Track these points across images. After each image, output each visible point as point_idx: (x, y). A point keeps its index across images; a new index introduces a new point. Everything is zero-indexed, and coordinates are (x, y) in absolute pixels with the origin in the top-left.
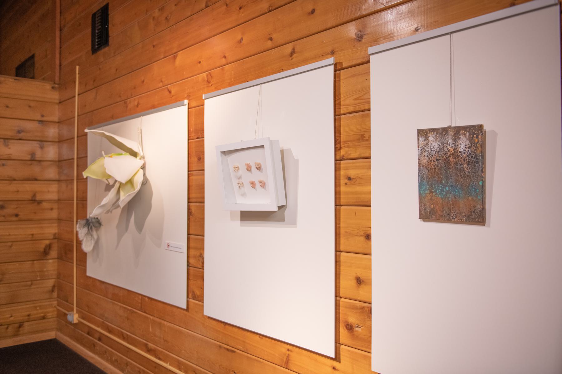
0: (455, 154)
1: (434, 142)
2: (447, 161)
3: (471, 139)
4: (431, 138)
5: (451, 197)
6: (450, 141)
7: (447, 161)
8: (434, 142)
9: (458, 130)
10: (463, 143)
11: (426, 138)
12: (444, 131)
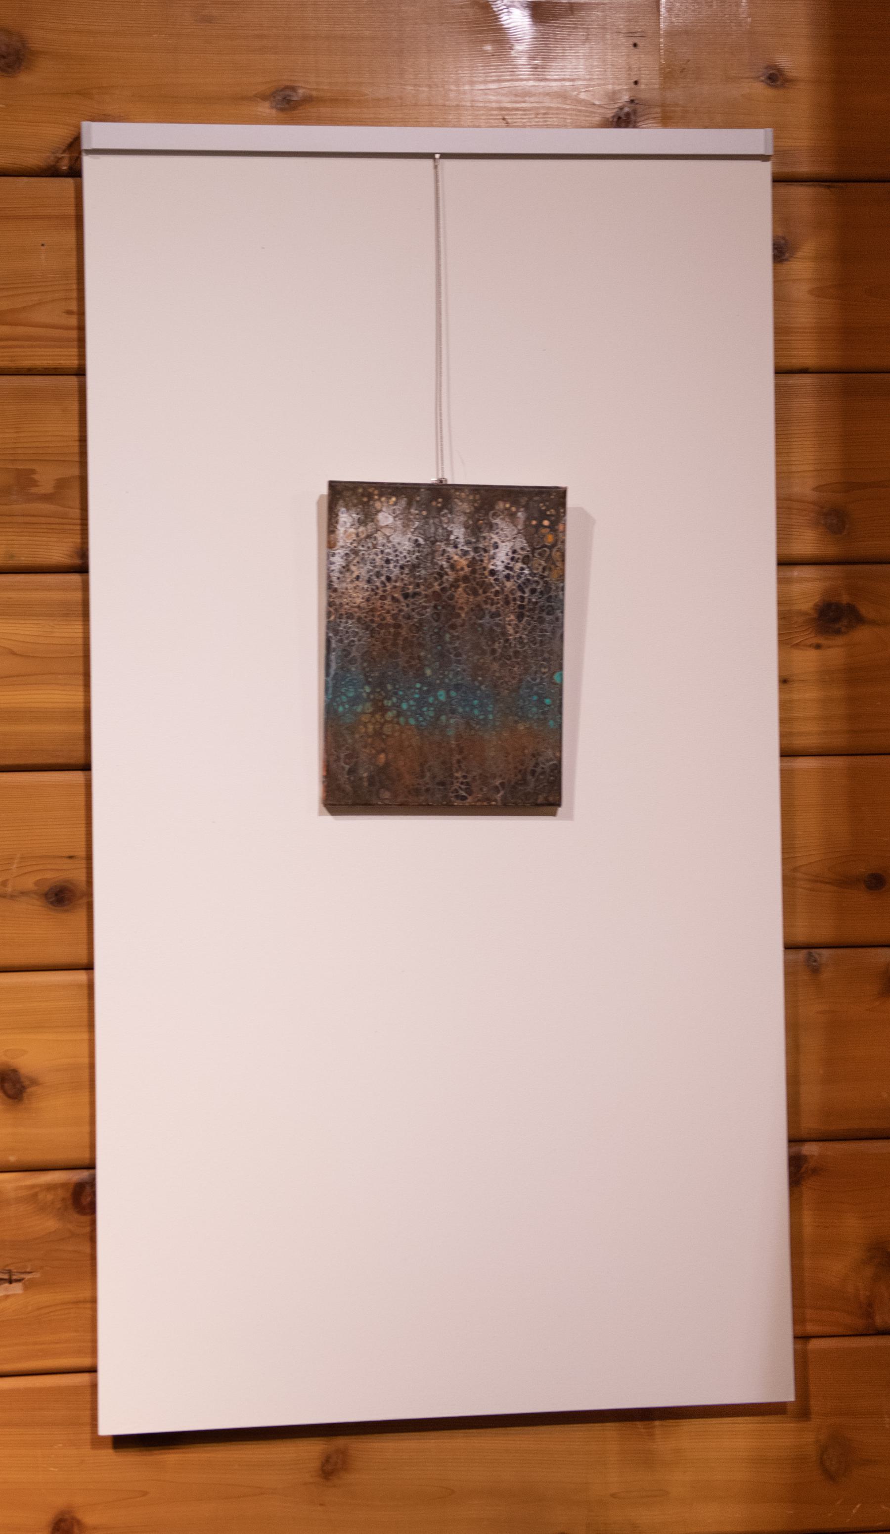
0: (476, 577)
2: (443, 603)
3: (531, 534)
4: (385, 518)
5: (453, 724)
6: (458, 533)
7: (443, 603)
9: (488, 500)
10: (504, 547)
11: (368, 517)
12: (439, 496)
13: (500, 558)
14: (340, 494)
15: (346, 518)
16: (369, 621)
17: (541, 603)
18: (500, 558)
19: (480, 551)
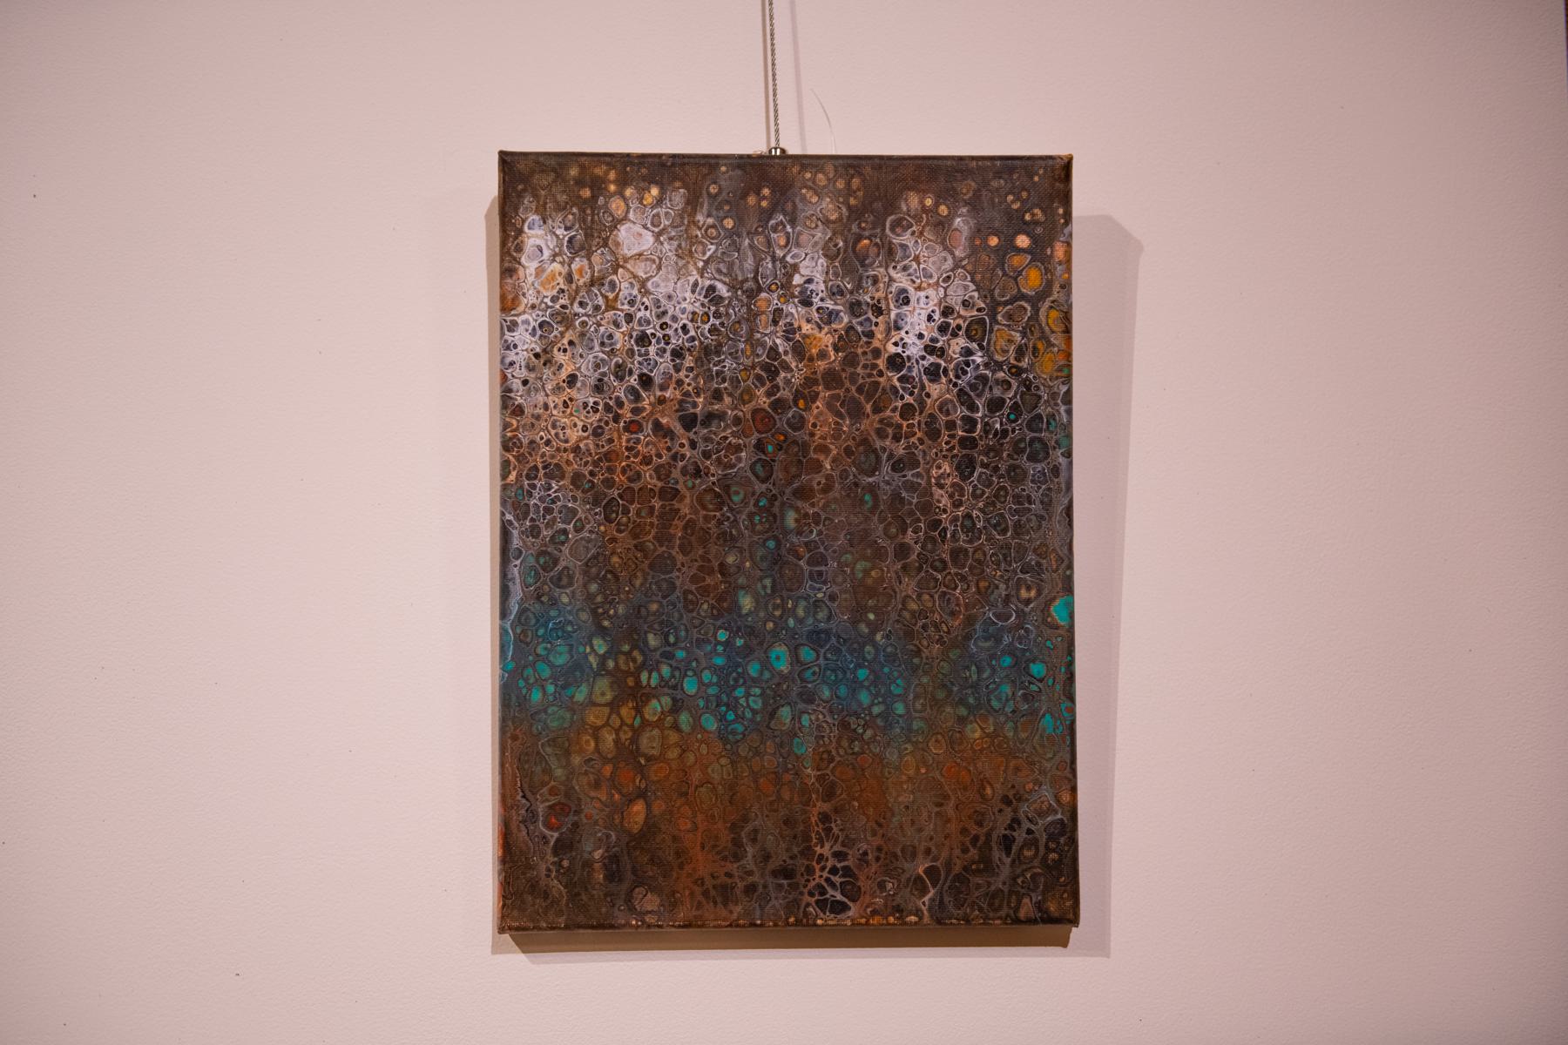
0: (858, 375)
1: (660, 270)
2: (780, 440)
3: (987, 268)
4: (634, 237)
5: (808, 727)
6: (812, 268)
8: (660, 270)
9: (882, 193)
10: (923, 295)
11: (593, 234)
13: (915, 327)
14: (525, 179)
15: (538, 237)
16: (606, 486)
17: (1014, 431)
18: (915, 327)
19: (866, 311)
